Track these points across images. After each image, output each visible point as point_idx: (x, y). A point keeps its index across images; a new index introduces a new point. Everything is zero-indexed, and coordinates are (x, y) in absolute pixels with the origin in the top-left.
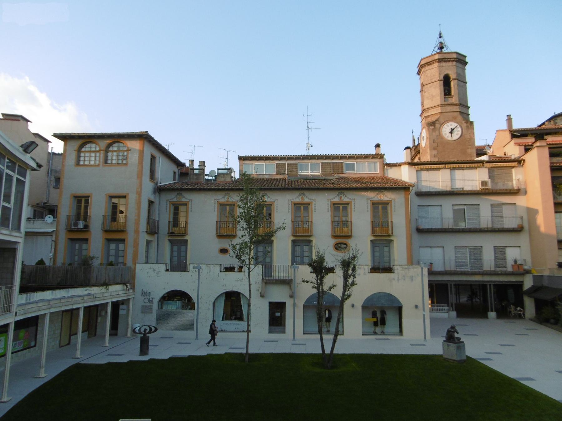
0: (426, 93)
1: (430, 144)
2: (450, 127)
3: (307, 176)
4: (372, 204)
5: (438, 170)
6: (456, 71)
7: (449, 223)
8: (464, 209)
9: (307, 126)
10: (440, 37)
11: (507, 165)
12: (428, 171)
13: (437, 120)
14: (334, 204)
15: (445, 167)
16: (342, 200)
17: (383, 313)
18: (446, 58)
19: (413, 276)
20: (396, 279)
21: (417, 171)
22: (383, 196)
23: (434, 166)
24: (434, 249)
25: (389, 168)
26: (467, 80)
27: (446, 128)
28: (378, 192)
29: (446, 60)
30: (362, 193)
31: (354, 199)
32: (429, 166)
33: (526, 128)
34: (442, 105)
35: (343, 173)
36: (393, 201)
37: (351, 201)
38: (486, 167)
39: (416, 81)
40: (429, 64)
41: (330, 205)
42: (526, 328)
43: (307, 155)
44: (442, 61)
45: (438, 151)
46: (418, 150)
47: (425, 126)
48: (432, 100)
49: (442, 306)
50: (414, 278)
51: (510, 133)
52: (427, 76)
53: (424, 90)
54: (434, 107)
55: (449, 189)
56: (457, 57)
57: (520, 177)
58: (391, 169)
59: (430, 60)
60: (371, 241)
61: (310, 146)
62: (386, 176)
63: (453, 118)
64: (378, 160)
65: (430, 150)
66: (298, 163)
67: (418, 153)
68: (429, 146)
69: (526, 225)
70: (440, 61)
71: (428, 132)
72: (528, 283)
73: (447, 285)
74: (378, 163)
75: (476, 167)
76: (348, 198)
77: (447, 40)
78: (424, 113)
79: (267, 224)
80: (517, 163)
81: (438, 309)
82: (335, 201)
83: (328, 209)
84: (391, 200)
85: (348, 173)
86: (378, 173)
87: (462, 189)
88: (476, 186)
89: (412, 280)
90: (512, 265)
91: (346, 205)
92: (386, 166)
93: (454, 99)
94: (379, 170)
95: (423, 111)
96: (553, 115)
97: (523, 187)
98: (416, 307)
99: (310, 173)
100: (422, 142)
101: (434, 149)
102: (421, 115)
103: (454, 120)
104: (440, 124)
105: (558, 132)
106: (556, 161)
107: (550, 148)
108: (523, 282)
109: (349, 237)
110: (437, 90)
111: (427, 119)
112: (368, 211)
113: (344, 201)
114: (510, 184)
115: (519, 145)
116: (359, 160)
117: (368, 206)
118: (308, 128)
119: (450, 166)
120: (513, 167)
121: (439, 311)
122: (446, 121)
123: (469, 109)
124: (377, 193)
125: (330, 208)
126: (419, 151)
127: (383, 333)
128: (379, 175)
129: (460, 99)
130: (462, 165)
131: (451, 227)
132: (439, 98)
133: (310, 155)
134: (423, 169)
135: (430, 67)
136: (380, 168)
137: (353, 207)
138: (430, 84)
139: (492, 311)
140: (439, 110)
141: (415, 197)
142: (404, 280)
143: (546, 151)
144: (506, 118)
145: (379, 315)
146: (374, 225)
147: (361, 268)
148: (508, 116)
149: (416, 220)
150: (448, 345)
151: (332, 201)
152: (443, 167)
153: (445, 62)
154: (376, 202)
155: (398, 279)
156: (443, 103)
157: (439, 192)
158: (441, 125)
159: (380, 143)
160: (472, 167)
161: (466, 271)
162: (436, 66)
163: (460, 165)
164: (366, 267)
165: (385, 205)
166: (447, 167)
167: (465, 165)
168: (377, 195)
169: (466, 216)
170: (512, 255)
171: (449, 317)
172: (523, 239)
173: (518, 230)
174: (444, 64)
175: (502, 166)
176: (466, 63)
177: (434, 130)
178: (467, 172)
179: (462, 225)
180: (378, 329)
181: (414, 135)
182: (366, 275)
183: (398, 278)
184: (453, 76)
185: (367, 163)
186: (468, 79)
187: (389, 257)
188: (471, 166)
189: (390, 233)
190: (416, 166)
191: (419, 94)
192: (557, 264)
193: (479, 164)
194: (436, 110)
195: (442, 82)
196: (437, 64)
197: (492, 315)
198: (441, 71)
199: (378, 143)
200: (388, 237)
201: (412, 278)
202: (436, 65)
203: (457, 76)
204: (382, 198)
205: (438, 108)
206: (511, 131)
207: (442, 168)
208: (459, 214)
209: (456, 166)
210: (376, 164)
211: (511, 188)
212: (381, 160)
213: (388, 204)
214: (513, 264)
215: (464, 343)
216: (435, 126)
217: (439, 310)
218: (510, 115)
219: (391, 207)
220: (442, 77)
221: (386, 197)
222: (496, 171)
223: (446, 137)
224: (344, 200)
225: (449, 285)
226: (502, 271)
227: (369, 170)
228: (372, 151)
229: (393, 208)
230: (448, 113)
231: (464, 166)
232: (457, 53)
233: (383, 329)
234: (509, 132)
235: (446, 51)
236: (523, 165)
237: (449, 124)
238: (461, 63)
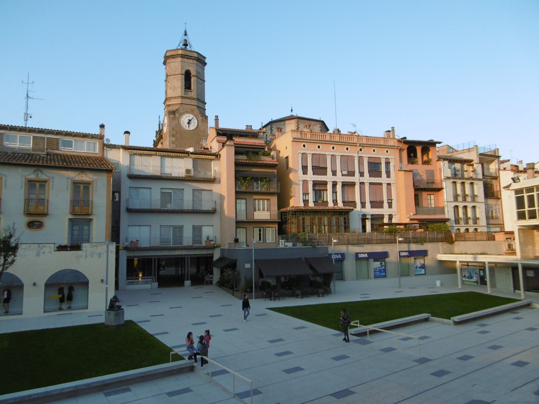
0: (169, 83)
1: (170, 131)
2: (189, 118)
3: (14, 149)
4: (72, 183)
5: (150, 156)
6: (196, 69)
7: (157, 204)
8: (171, 192)
9: (26, 94)
10: (186, 35)
11: (208, 158)
12: (140, 156)
13: (177, 110)
14: (29, 181)
15: (156, 154)
16: (40, 177)
17: (71, 289)
18: (188, 55)
19: (100, 253)
20: (84, 256)
21: (130, 155)
22: (84, 176)
23: (146, 152)
24: (142, 228)
25: (109, 149)
26: (206, 79)
27: (184, 119)
28: (80, 172)
29: (188, 57)
30: (62, 172)
31: (53, 177)
32: (142, 152)
33: (225, 128)
34: (182, 97)
35: (59, 150)
36: (95, 182)
37: (49, 179)
38: (191, 158)
39: (162, 70)
40: (173, 57)
41: (24, 181)
42: (206, 292)
43: (25, 127)
44: (184, 57)
45: (176, 138)
46: (161, 135)
47: (167, 114)
48: (174, 91)
50: (102, 255)
51: (216, 131)
52: (171, 68)
53: (167, 80)
54: (175, 98)
55: (158, 174)
56: (198, 57)
57: (217, 169)
58: (111, 150)
59: (174, 53)
60: (70, 219)
61: (29, 116)
62: (105, 156)
64: (97, 140)
65: (169, 136)
66: (4, 133)
67: (161, 138)
68: (168, 132)
69: (218, 208)
70: (183, 56)
71: (168, 120)
72: (217, 255)
73: (152, 259)
74: (98, 144)
75: (183, 157)
76: (46, 175)
77: (191, 40)
78: (167, 102)
80: (215, 157)
81: (131, 282)
82: (30, 178)
83: (22, 186)
84: (93, 180)
85: (64, 150)
87: (170, 175)
88: (182, 173)
90: (205, 241)
91: (43, 183)
92: (105, 147)
93: (193, 94)
95: (166, 100)
97: (218, 177)
98: (102, 281)
99: (19, 145)
100: (164, 128)
101: (173, 136)
102: (164, 103)
103: (192, 112)
104: (179, 114)
105: (249, 135)
106: (240, 158)
107: (235, 147)
108: (213, 254)
109: (45, 215)
110: (178, 83)
111: (169, 107)
112: (67, 190)
113: (40, 179)
114: (210, 174)
115: (219, 142)
116: (77, 138)
117: (68, 185)
118: (28, 96)
119: (161, 153)
120: (212, 160)
121: (133, 284)
122: (184, 112)
123: (205, 105)
124: (78, 173)
125: (23, 184)
126: (162, 136)
127: (69, 308)
128: (98, 156)
129: (198, 94)
130: (171, 154)
131: (157, 208)
132: (180, 90)
133: (29, 127)
134: (136, 154)
135: (174, 60)
136: (99, 149)
137: (51, 185)
138: (173, 76)
139: (188, 280)
140: (179, 101)
141: (127, 178)
142: (92, 256)
143: (233, 150)
144: (215, 118)
145: (66, 292)
146: (74, 203)
147: (46, 247)
148: (216, 116)
149: (127, 200)
150: (109, 313)
151: (27, 177)
152: (154, 154)
153: (187, 58)
154: (77, 181)
155: (86, 256)
156: (183, 95)
157: (148, 176)
158: (180, 115)
160: (179, 156)
161: (167, 247)
162: (179, 61)
163: (169, 153)
164: (52, 246)
165: (87, 185)
166: (157, 154)
167: (174, 154)
168: (79, 175)
169: (172, 199)
170: (207, 232)
171: (151, 288)
172: (215, 220)
173: (213, 212)
174: (186, 60)
175: (203, 158)
176: (205, 64)
177: (174, 119)
178: (175, 160)
179: (169, 207)
180: (64, 306)
182: (51, 253)
183: (86, 255)
184: (193, 73)
185: (86, 142)
186: (206, 78)
187: (89, 235)
188: (179, 156)
189: (90, 212)
190: (130, 151)
191: (165, 83)
192: (234, 239)
193: (185, 155)
194: (177, 100)
195: (183, 76)
196: (180, 58)
197: (188, 283)
198: (183, 66)
199: (103, 124)
200: (87, 216)
201: (100, 255)
202: (179, 59)
203: (196, 74)
204: (84, 178)
205: (178, 99)
206: (216, 130)
207: (154, 155)
208: (166, 196)
209: (166, 154)
210: (96, 144)
211: (209, 177)
212: (101, 141)
213: (90, 184)
214: (206, 240)
215: (124, 309)
216: (175, 115)
217: (130, 283)
219: (93, 188)
220: (184, 72)
221: (86, 177)
222: (199, 161)
223: (184, 126)
224: (42, 178)
225: (153, 260)
226: (197, 246)
227: (88, 149)
228: (96, 131)
229: (94, 188)
231: (172, 154)
232: (197, 53)
233: (70, 305)
234: (215, 130)
235: (190, 49)
236: (219, 159)
237: (187, 115)
238: (201, 63)
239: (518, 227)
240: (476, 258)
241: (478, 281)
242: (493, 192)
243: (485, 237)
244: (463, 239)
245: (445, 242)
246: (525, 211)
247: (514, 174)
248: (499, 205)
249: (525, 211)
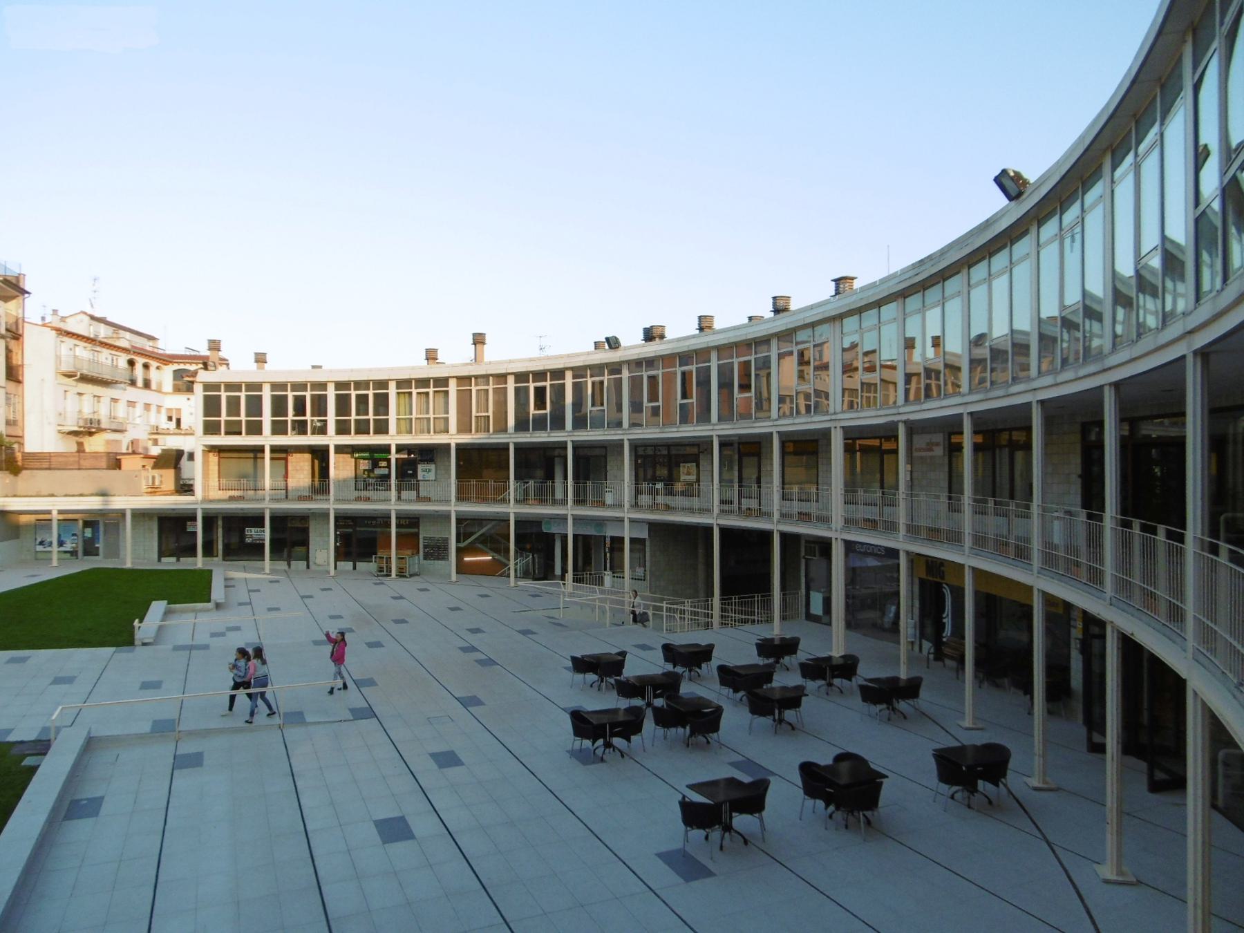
239: (202, 446)
240: (109, 503)
241: (76, 549)
242: (980, 454)
243: (104, 464)
244: (45, 465)
245: (6, 470)
246: (220, 421)
247: (57, 337)
248: (19, 396)
249: (220, 421)
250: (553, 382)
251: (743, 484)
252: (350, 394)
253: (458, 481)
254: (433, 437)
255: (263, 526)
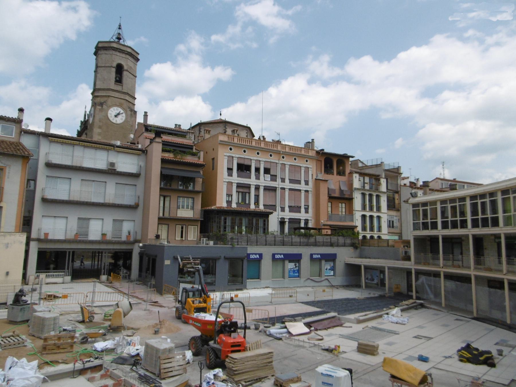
10: (120, 28)
11: (134, 153)
13: (105, 102)
48: (103, 83)
49: (58, 272)
50: (9, 245)
63: (120, 104)
73: (66, 252)
74: (14, 128)
79: (489, 215)
80: (141, 152)
86: (13, 138)
89: (7, 247)
94: (14, 135)
96: (200, 122)
103: (120, 106)
107: (163, 144)
108: (132, 249)
139: (104, 274)
144: (143, 114)
153: (119, 52)
159: (24, 108)
166: (81, 144)
181: (86, 110)
191: (93, 73)
212: (18, 125)
216: (102, 107)
218: (147, 112)
225: (68, 253)
226: (115, 241)
230: (116, 99)
235: (123, 43)
237: (115, 108)
250: (460, 203)
251: (454, 255)
252: (447, 206)
253: (444, 255)
254: (451, 231)
255: (471, 283)
